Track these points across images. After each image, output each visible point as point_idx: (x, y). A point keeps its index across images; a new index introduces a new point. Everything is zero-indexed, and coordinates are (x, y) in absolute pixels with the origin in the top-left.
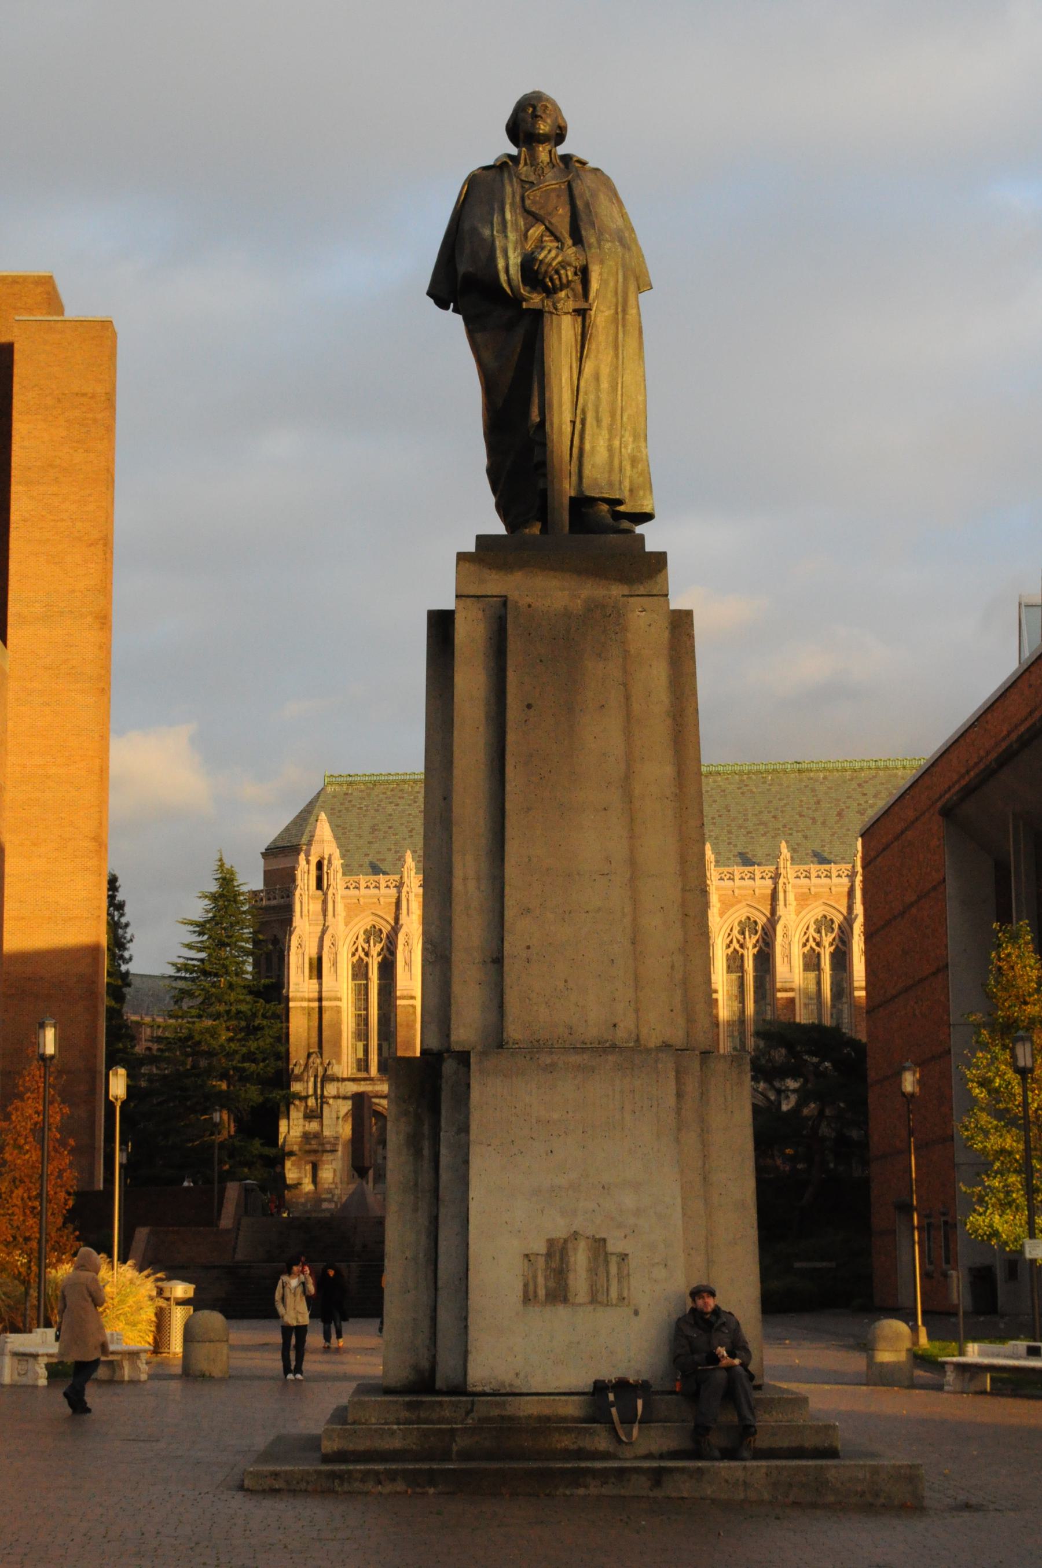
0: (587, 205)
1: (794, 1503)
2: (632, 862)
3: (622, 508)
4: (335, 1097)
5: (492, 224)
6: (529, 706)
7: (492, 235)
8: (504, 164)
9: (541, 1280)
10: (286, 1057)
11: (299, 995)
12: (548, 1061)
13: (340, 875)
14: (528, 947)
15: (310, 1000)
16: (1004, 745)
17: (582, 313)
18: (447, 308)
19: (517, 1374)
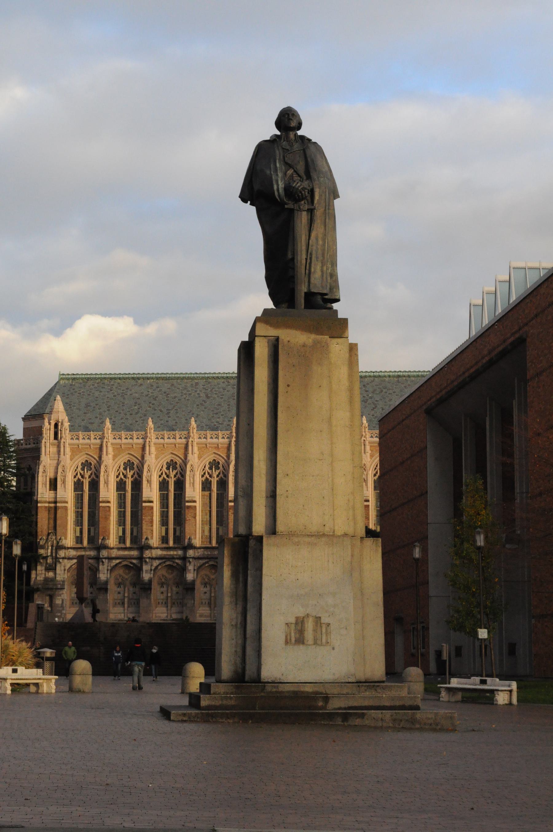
0: (313, 161)
1: (403, 728)
2: (332, 455)
3: (326, 297)
4: (63, 558)
5: (270, 169)
6: (288, 386)
7: (271, 174)
8: (275, 140)
9: (293, 634)
10: (36, 535)
11: (43, 499)
12: (297, 541)
13: (68, 431)
14: (287, 491)
15: (49, 503)
16: (461, 379)
17: (311, 212)
18: (247, 202)
19: (282, 674)
